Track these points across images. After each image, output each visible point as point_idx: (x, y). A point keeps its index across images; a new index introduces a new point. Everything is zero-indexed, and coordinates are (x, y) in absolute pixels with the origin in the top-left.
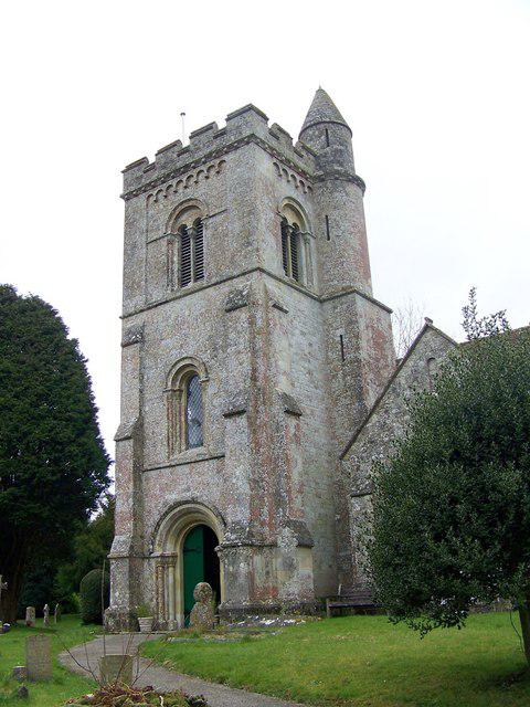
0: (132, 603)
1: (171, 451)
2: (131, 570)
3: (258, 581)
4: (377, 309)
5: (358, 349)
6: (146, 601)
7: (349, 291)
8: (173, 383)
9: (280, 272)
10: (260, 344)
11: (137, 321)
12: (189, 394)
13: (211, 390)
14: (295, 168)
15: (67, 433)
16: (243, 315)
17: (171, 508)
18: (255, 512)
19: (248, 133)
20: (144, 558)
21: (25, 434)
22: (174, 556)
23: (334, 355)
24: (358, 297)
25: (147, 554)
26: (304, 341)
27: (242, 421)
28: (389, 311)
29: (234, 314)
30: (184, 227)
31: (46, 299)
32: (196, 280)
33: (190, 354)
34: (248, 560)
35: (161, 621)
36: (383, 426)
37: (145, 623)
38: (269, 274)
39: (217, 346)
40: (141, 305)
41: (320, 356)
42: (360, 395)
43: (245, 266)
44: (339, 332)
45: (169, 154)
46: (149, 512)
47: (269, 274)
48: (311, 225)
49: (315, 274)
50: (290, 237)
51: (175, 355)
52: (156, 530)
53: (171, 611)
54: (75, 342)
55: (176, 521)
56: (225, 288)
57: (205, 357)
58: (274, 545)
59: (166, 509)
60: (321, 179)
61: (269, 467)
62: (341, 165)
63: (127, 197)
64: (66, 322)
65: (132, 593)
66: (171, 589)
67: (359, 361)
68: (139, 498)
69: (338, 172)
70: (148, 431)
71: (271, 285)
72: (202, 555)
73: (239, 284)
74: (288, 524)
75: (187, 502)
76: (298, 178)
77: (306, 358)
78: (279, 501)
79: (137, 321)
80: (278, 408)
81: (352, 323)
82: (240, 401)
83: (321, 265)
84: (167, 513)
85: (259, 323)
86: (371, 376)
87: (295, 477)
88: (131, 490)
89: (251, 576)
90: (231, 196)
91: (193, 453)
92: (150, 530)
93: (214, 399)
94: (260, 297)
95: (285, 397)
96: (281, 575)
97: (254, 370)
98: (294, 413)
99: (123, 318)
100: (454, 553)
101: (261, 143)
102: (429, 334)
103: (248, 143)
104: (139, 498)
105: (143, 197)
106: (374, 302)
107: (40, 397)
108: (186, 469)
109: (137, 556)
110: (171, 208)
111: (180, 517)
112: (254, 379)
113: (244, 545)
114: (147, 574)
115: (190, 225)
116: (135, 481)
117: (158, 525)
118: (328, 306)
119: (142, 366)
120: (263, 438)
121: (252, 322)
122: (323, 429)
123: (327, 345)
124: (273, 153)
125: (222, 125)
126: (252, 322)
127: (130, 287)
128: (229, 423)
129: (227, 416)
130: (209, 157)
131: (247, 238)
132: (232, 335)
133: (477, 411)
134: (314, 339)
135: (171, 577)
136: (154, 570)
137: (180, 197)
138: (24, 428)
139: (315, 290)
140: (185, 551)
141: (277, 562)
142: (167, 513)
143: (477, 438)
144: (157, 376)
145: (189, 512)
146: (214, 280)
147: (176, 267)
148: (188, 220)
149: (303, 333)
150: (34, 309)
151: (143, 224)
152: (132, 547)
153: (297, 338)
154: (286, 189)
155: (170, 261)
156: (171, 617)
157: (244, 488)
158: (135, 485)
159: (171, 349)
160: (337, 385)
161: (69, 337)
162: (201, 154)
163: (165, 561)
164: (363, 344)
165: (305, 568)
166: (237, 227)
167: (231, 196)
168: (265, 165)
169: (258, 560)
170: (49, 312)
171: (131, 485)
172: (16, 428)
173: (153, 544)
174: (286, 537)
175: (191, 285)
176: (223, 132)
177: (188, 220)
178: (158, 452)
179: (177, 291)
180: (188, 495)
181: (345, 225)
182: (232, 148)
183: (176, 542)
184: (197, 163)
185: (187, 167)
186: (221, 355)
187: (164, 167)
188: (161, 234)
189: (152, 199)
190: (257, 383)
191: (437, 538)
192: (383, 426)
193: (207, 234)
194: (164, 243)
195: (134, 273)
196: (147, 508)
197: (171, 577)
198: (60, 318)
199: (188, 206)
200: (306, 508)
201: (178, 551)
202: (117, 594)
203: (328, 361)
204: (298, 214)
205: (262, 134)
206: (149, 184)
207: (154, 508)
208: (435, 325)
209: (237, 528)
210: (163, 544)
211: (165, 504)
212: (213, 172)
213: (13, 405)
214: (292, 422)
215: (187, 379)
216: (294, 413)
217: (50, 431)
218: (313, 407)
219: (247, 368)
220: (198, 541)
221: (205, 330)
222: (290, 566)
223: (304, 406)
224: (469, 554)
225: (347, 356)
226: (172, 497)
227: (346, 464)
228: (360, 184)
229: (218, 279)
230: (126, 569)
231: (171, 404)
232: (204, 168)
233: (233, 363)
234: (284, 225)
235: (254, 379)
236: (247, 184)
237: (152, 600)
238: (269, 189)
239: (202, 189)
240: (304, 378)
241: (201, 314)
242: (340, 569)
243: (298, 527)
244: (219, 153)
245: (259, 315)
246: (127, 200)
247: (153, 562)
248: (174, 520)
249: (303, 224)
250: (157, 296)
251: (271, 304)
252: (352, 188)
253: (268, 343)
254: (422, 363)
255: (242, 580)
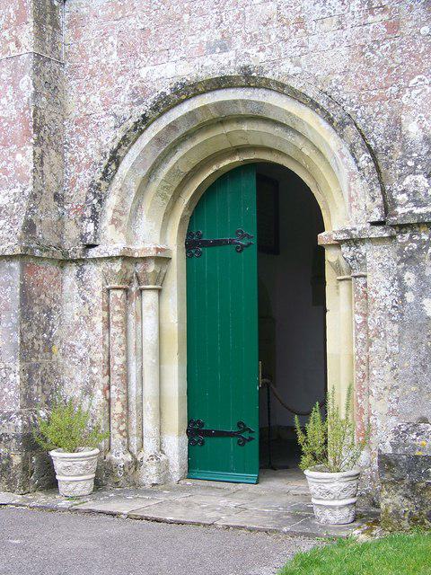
0: (29, 401)
2: (26, 297)
6: (71, 391)
17: (164, 105)
20: (64, 262)
22: (162, 260)
25: (73, 247)
35: (120, 457)
37: (72, 469)
46: (83, 121)
52: (107, 176)
53: (149, 426)
55: (173, 148)
59: (140, 110)
65: (29, 373)
66: (149, 358)
72: (252, 253)
84: (146, 121)
92: (85, 178)
111: (189, 136)
114: (72, 310)
116: (39, 23)
117: (115, 159)
136: (97, 298)
140: (192, 244)
142: (146, 121)
143: (402, 106)
145: (223, 117)
152: (30, 227)
156: (150, 446)
158: (40, 35)
173: (95, 217)
183: (168, 215)
196: (74, 111)
201: (173, 243)
211: (137, 96)
220: (241, 214)
226: (165, 72)
237: (88, 391)
247: (94, 274)
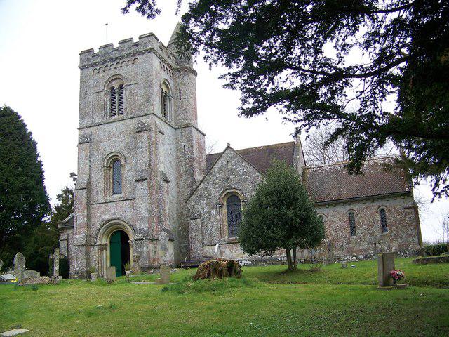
1: (106, 196)
3: (151, 255)
4: (200, 134)
5: (192, 153)
7: (189, 126)
8: (107, 163)
9: (160, 114)
10: (153, 149)
11: (88, 131)
12: (114, 168)
13: (127, 168)
14: (168, 64)
15: (33, 183)
16: (145, 135)
17: (106, 222)
18: (150, 225)
19: (150, 47)
21: (11, 184)
22: (106, 245)
23: (181, 155)
24: (193, 129)
26: (168, 147)
27: (145, 183)
28: (205, 135)
29: (140, 134)
30: (113, 88)
31: (16, 108)
32: (119, 115)
33: (117, 150)
34: (147, 245)
36: (206, 189)
38: (157, 116)
39: (132, 147)
40: (89, 123)
41: (174, 155)
42: (192, 174)
43: (146, 111)
44: (184, 144)
45: (107, 50)
47: (157, 116)
48: (173, 92)
49: (173, 117)
50: (164, 97)
51: (108, 150)
54: (31, 133)
56: (136, 121)
57: (124, 152)
58: (158, 240)
60: (178, 70)
61: (157, 204)
62: (188, 64)
63: (82, 68)
64: (26, 122)
67: (192, 158)
68: (89, 217)
69: (186, 67)
70: (93, 186)
71: (158, 121)
73: (143, 120)
74: (164, 230)
75: (115, 220)
76: (169, 69)
77: (170, 155)
78: (160, 220)
79: (88, 131)
80: (160, 179)
81: (190, 140)
82: (144, 174)
83: (176, 112)
85: (153, 139)
86: (197, 165)
87: (167, 209)
88: (86, 213)
89: (148, 253)
90: (140, 77)
91: (117, 197)
93: (128, 173)
94: (153, 126)
95: (163, 174)
96: (161, 252)
97: (150, 161)
98: (167, 181)
99: (79, 129)
100: (274, 233)
101: (155, 52)
102: (229, 150)
103: (149, 52)
104: (89, 217)
105: (91, 69)
106: (199, 131)
107: (19, 164)
108: (114, 204)
109: (89, 244)
110: (107, 77)
112: (150, 165)
113: (146, 239)
114: (93, 253)
115: (116, 87)
117: (99, 230)
118: (179, 131)
119: (91, 154)
120: (154, 192)
121: (149, 138)
122: (175, 189)
123: (177, 149)
124: (160, 57)
125: (136, 40)
126: (149, 138)
127: (83, 114)
128: (138, 184)
129: (137, 181)
130: (129, 55)
131: (148, 98)
132: (140, 144)
133: (279, 192)
134: (173, 147)
135: (105, 254)
137: (112, 72)
138: (11, 180)
139: (173, 124)
141: (159, 247)
144: (97, 159)
145: (115, 224)
146: (129, 116)
147: (108, 107)
148: (116, 85)
149: (168, 144)
150: (9, 115)
151: (91, 83)
153: (167, 146)
154: (164, 75)
155: (105, 103)
157: (146, 214)
159: (107, 147)
160: (182, 168)
161: (28, 131)
162: (124, 53)
163: (102, 247)
164: (195, 150)
165: (171, 249)
166: (142, 92)
167: (140, 77)
168: (156, 62)
169: (151, 246)
170: (17, 116)
171: (85, 211)
172: (7, 181)
174: (163, 236)
175: (116, 117)
176: (137, 44)
177: (116, 85)
178: (99, 195)
179: (109, 119)
180: (115, 216)
181: (188, 94)
182: (142, 53)
184: (122, 57)
185: (117, 58)
186: (133, 152)
187: (104, 56)
188: (101, 89)
189: (96, 71)
190: (151, 168)
191: (268, 228)
192: (206, 189)
193: (126, 93)
194: (103, 94)
195: (85, 107)
197: (105, 254)
198: (22, 121)
199: (116, 78)
200: (169, 223)
201: (108, 242)
202: (79, 263)
203: (177, 157)
204: (167, 87)
205: (156, 48)
206: (95, 63)
207: (96, 223)
208: (231, 146)
209: (142, 231)
210: (101, 239)
211: (103, 220)
212: (130, 63)
213: (4, 168)
214: (166, 185)
215: (114, 162)
216: (167, 181)
217: (23, 182)
218: (172, 178)
219: (147, 159)
220: (119, 237)
221: (125, 140)
222: (165, 249)
223: (170, 178)
224: (279, 233)
225: (187, 156)
226: (106, 217)
227: (188, 205)
228: (195, 73)
229: (132, 116)
230: (84, 251)
231: (105, 174)
232: (126, 60)
233: (139, 157)
234: (162, 92)
235: (150, 165)
236: (149, 72)
238: (158, 75)
239: (124, 70)
240: (168, 165)
241: (123, 132)
242: (181, 252)
243: (168, 231)
244: (134, 54)
245: (153, 135)
246: (82, 69)
248: (107, 228)
249: (169, 92)
250: (98, 120)
251: (158, 130)
252: (192, 76)
253: (157, 149)
254: (225, 163)
255: (145, 255)
